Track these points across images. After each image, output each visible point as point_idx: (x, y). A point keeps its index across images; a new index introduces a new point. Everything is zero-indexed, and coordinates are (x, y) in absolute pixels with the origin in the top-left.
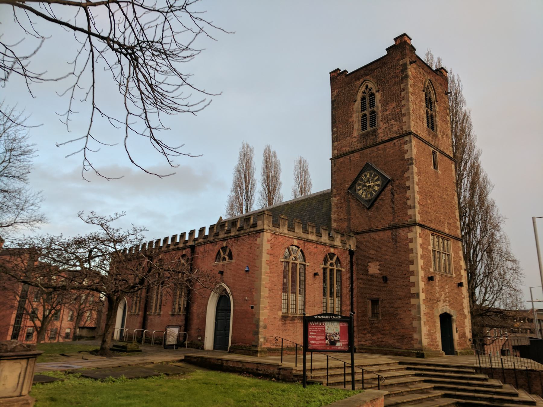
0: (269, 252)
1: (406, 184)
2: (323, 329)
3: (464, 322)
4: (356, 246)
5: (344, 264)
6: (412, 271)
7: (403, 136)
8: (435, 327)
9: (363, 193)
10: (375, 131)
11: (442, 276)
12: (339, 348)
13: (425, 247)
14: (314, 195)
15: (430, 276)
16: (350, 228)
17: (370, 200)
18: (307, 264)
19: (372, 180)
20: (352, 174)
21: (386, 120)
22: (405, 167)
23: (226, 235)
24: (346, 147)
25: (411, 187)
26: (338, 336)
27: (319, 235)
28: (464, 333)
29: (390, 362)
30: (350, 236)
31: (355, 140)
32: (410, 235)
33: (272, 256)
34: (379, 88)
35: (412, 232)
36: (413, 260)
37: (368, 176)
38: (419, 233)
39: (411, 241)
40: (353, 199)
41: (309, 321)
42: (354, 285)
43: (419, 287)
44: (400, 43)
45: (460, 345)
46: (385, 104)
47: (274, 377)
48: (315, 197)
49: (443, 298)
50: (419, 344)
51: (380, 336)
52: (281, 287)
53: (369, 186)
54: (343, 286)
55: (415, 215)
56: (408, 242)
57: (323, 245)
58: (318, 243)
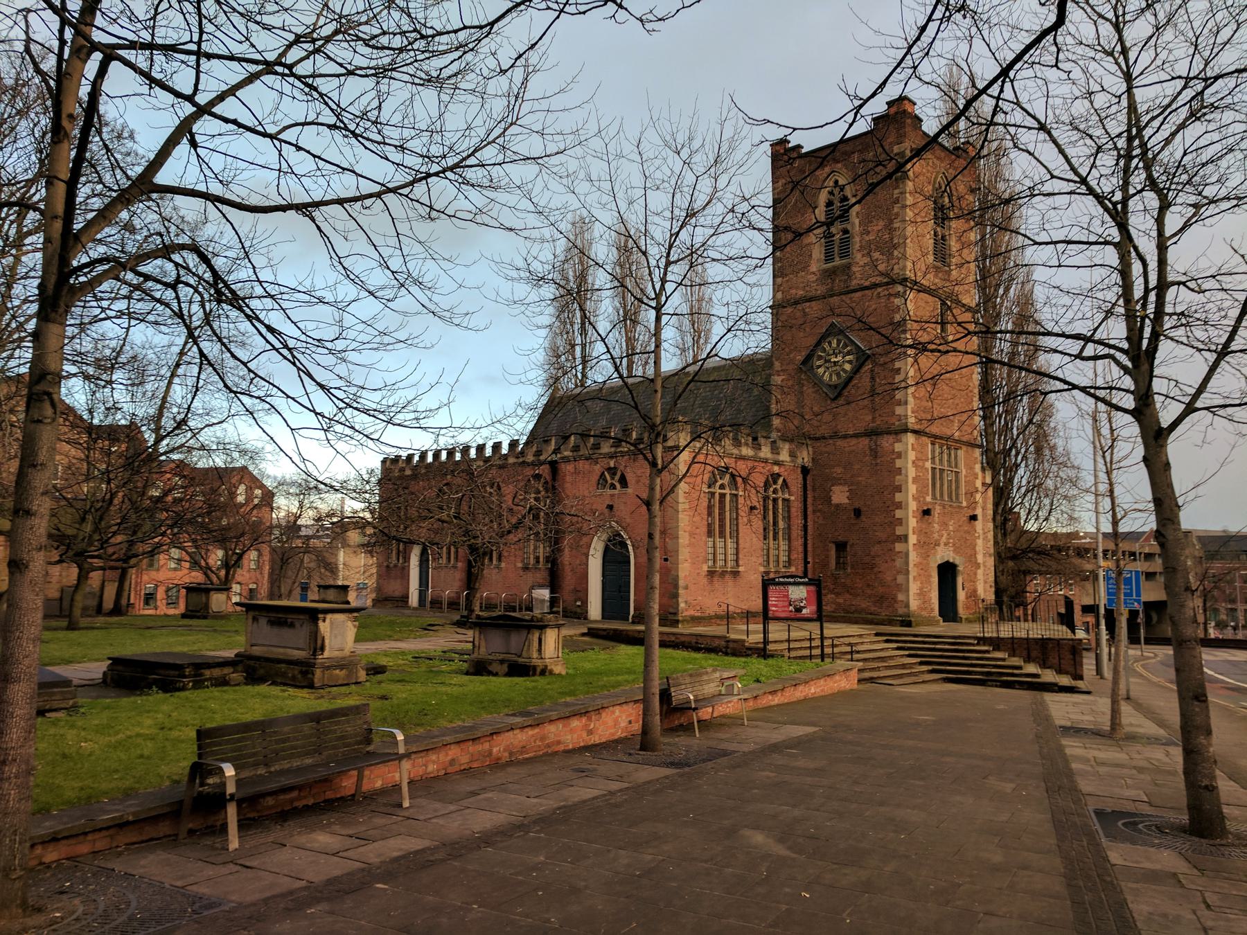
3: (975, 574)
4: (813, 459)
7: (893, 282)
8: (930, 583)
10: (848, 267)
11: (944, 508)
15: (925, 508)
17: (835, 386)
19: (840, 352)
21: (867, 249)
23: (613, 450)
24: (797, 288)
27: (758, 447)
28: (975, 591)
31: (813, 278)
32: (898, 447)
34: (856, 191)
37: (834, 344)
39: (899, 455)
41: (769, 584)
44: (896, 113)
45: (968, 608)
46: (866, 221)
47: (721, 651)
49: (944, 539)
51: (848, 596)
52: (705, 529)
53: (835, 362)
58: (755, 459)
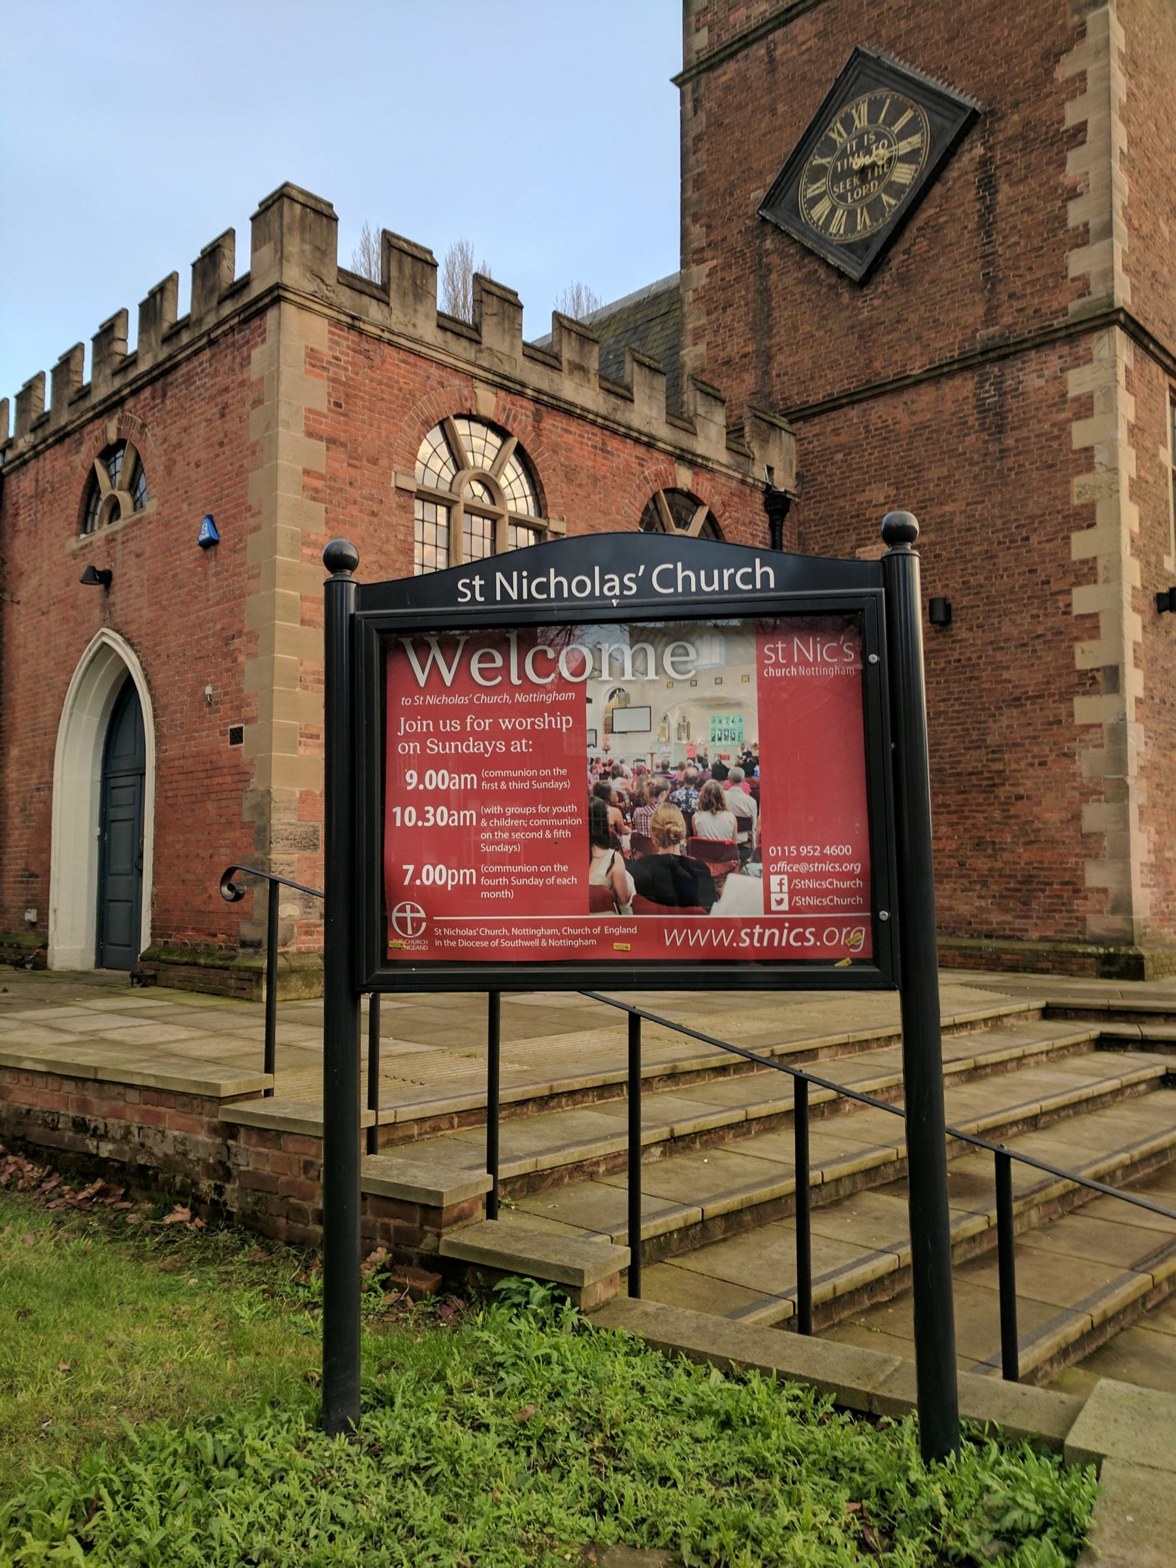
0: (324, 428)
1: (1062, 121)
2: (564, 723)
4: (799, 476)
6: (1084, 562)
9: (833, 211)
13: (1148, 444)
14: (606, 314)
16: (770, 394)
17: (866, 244)
19: (879, 136)
20: (780, 128)
22: (1063, 27)
25: (1090, 127)
26: (738, 799)
29: (1003, 1010)
30: (773, 425)
32: (1078, 382)
33: (340, 454)
35: (1091, 361)
36: (1090, 507)
37: (861, 123)
38: (1127, 369)
40: (783, 256)
43: (1120, 635)
48: (613, 317)
50: (1115, 910)
53: (863, 170)
55: (1108, 274)
56: (1063, 416)
57: (637, 441)
58: (609, 427)
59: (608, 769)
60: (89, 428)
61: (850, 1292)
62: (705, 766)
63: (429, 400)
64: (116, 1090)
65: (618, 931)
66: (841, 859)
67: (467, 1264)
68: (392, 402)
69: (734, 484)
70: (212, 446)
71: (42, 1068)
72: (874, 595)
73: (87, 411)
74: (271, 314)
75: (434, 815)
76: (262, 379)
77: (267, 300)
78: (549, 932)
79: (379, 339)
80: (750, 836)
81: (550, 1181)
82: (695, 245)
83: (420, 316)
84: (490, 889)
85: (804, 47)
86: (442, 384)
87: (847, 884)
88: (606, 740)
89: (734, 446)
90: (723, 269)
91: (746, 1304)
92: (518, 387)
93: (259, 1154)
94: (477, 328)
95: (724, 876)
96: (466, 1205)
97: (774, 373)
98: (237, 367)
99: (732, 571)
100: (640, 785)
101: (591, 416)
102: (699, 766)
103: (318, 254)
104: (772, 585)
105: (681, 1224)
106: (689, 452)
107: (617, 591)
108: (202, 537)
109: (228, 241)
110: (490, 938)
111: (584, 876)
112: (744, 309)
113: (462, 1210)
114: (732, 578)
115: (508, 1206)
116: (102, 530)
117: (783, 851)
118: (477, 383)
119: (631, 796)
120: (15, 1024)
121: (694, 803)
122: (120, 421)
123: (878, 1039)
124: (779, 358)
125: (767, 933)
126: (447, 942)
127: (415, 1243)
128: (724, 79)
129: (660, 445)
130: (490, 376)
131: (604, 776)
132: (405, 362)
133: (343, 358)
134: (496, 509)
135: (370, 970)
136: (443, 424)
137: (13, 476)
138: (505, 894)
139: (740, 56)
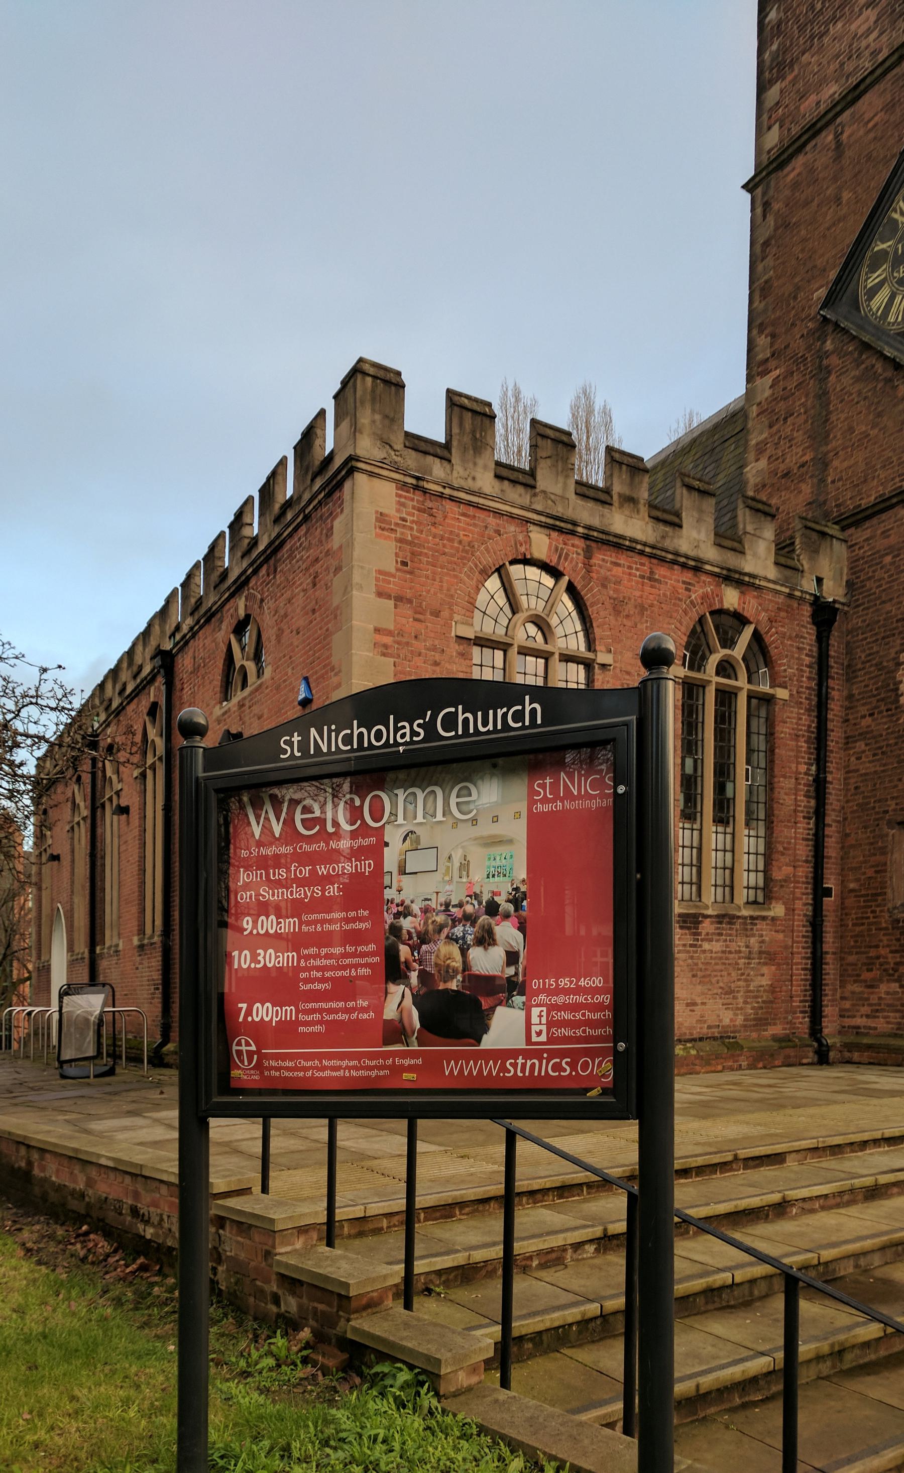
0: (392, 587)
4: (850, 585)
5: (787, 666)
12: (515, 1070)
16: (825, 502)
18: (603, 657)
30: (823, 534)
33: (406, 609)
42: (831, 767)
48: (694, 441)
54: (777, 771)
57: (684, 566)
59: (400, 909)
60: (227, 607)
61: (718, 1390)
62: (480, 903)
63: (487, 549)
64: (156, 1184)
65: (407, 1062)
66: (594, 991)
67: (367, 1347)
68: (453, 556)
69: (781, 599)
70: (307, 614)
71: (111, 1164)
72: (627, 724)
73: (224, 592)
74: (347, 485)
75: (264, 958)
76: (341, 547)
77: (343, 473)
78: (352, 1063)
79: (441, 496)
80: (517, 969)
81: (484, 1272)
82: (760, 357)
83: (479, 469)
84: (306, 1024)
85: (870, 125)
86: (498, 532)
87: (598, 1016)
88: (399, 881)
89: (782, 560)
90: (785, 378)
91: (606, 1397)
92: (569, 526)
93: (238, 1242)
94: (532, 473)
95: (492, 1009)
96: (375, 1294)
97: (829, 480)
98: (324, 538)
99: (505, 710)
100: (426, 923)
101: (639, 547)
102: (476, 903)
103: (387, 422)
104: (539, 722)
105: (579, 1318)
106: (736, 572)
107: (408, 738)
108: (301, 697)
109: (319, 421)
110: (305, 1069)
111: (380, 1010)
112: (803, 417)
113: (372, 1298)
114: (505, 716)
115: (439, 1294)
116: (239, 696)
117: (544, 983)
118: (532, 528)
119: (419, 934)
120: (147, 1122)
121: (469, 938)
122: (246, 599)
123: (852, 1144)
124: (835, 463)
125: (529, 1063)
126: (273, 1073)
127: (333, 1325)
128: (792, 176)
129: (708, 567)
130: (543, 519)
131: (397, 915)
132: (464, 515)
133: (409, 518)
134: (548, 648)
135: (209, 1096)
136: (499, 570)
137: (180, 656)
138: (317, 1028)
139: (809, 147)
